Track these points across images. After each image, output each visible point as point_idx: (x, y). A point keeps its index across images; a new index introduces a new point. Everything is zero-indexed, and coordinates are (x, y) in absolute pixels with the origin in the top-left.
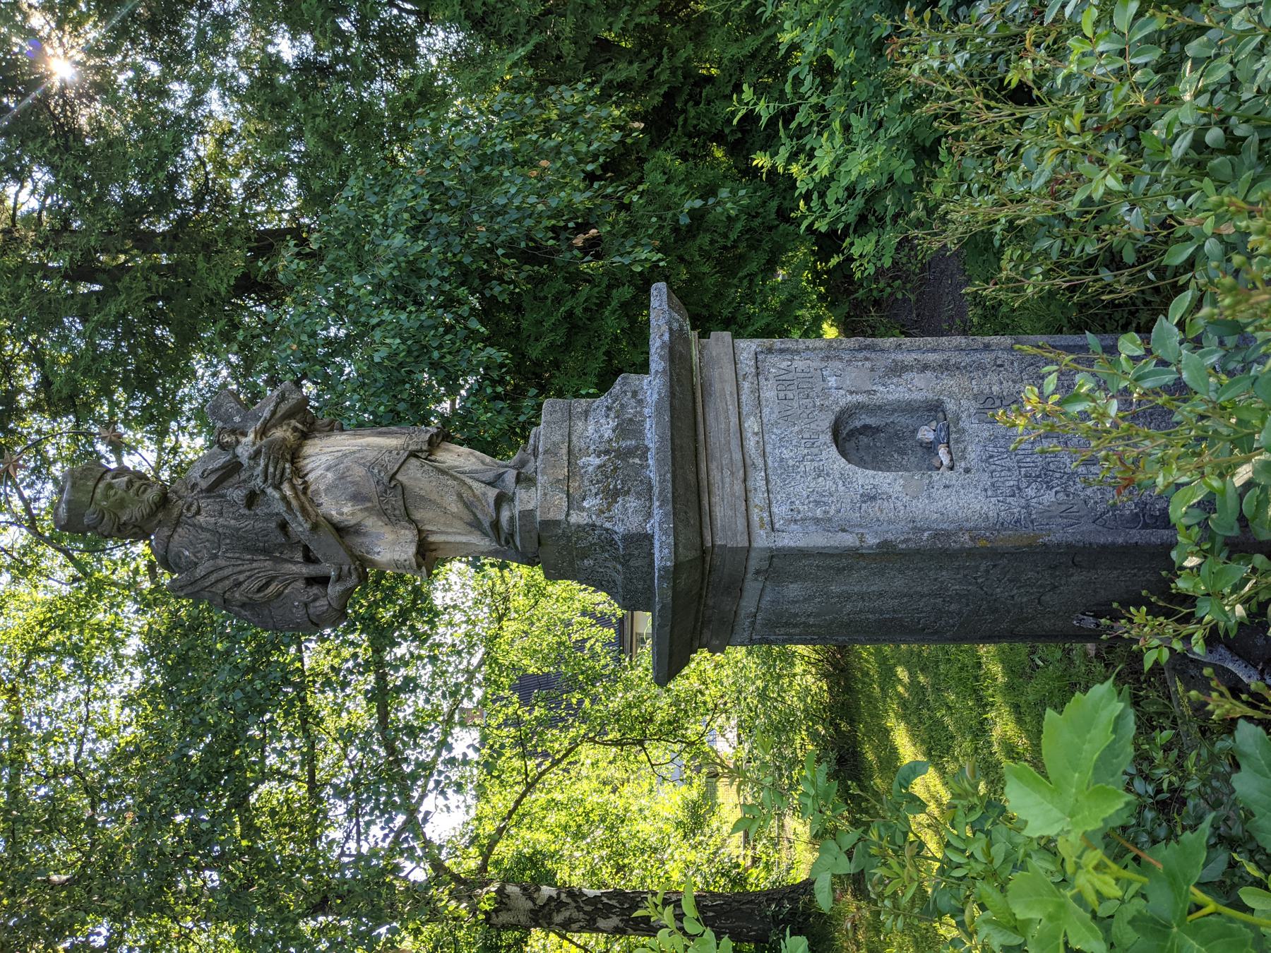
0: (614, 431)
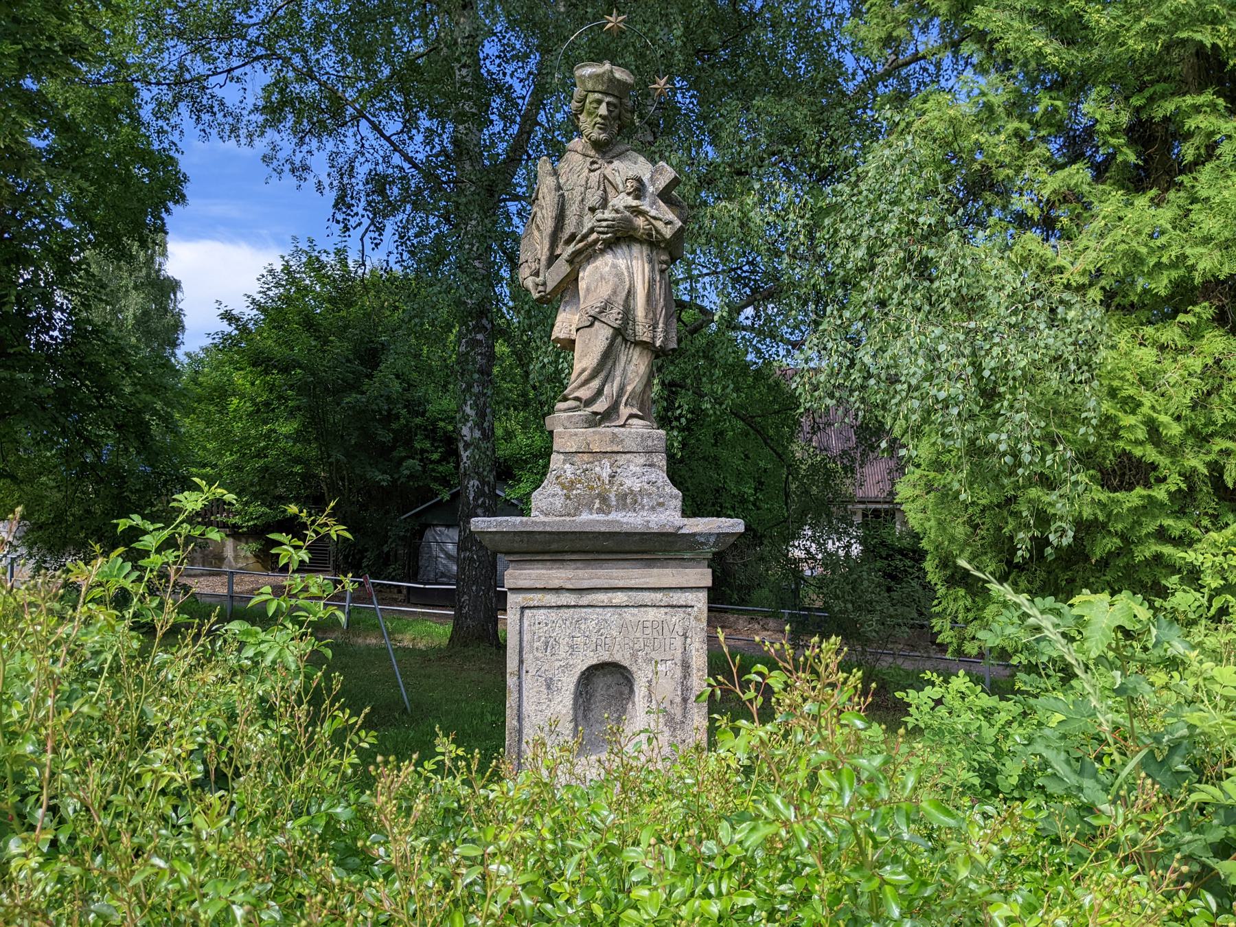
0: (629, 488)
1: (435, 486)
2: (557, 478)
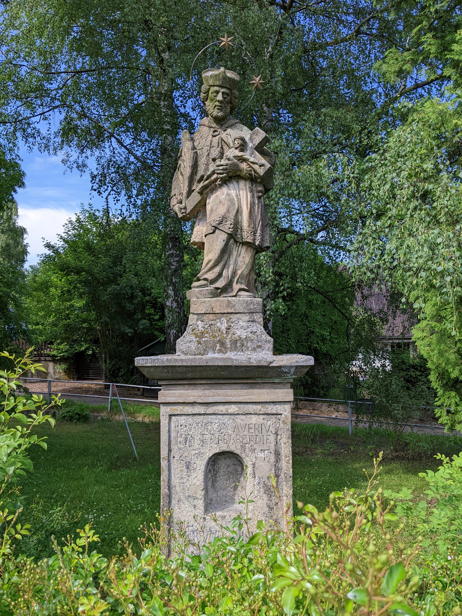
0: (239, 336)
1: (156, 333)
2: (193, 330)
